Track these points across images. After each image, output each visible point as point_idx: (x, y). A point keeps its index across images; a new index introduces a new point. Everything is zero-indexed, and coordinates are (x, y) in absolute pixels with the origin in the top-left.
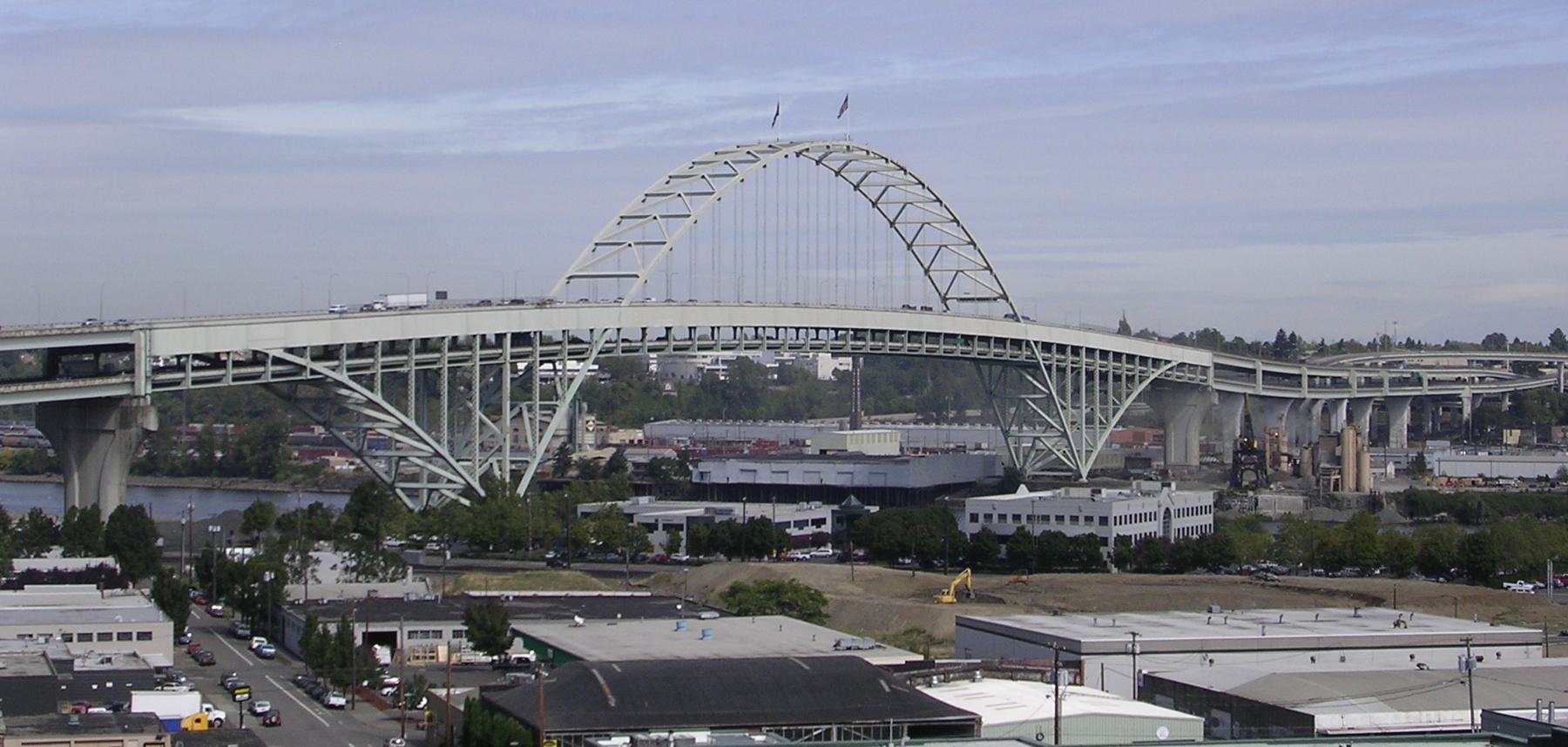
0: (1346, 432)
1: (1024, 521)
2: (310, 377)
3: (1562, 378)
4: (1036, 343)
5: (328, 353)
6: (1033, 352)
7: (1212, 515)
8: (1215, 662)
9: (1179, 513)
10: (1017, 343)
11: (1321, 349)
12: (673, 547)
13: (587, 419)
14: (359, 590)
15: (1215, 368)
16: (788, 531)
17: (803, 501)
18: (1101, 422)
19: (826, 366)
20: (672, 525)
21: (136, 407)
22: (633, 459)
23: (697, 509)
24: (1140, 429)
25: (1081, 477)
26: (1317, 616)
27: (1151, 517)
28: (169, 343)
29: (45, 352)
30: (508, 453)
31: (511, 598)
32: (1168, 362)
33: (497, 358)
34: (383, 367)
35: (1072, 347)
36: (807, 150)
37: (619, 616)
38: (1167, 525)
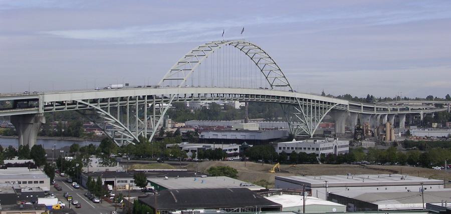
5: (94, 101)
10: (292, 98)
11: (380, 100)
12: (194, 157)
14: (103, 169)
19: (238, 105)
23: (201, 146)
28: (49, 98)
38: (335, 151)
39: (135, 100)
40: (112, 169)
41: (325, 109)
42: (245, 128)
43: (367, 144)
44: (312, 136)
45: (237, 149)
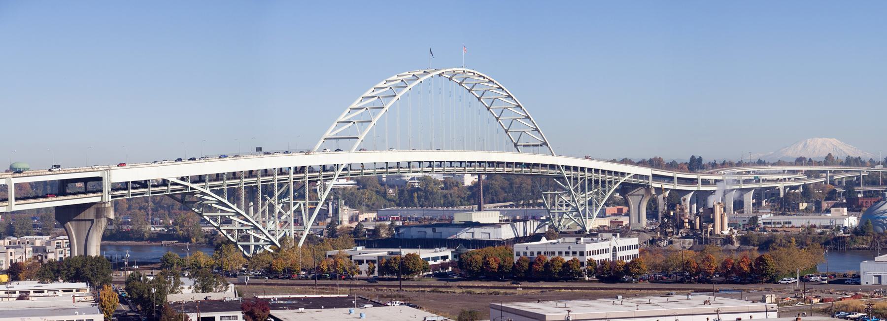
0: (716, 207)
1: (557, 255)
2: (190, 191)
3: (828, 178)
4: (562, 166)
5: (200, 179)
6: (561, 171)
7: (638, 249)
8: (710, 319)
9: (621, 249)
10: (553, 167)
11: (714, 165)
12: (371, 271)
13: (344, 208)
14: (201, 296)
15: (653, 176)
16: (429, 262)
17: (437, 247)
18: (596, 204)
19: (469, 180)
20: (370, 260)
21: (104, 208)
22: (366, 228)
23: (383, 252)
24: (620, 207)
25: (586, 231)
26: (667, 300)
27: (605, 251)
28: (120, 175)
29: (60, 181)
30: (293, 226)
31: (276, 299)
32: (628, 174)
33: (286, 180)
34: (309, 178)
35: (581, 167)
36: (443, 73)
37: (323, 307)
38: (614, 255)
39: (288, 174)
40: (214, 296)
41: (610, 182)
42: (474, 220)
43: (682, 245)
44: (588, 230)
45: (447, 257)
